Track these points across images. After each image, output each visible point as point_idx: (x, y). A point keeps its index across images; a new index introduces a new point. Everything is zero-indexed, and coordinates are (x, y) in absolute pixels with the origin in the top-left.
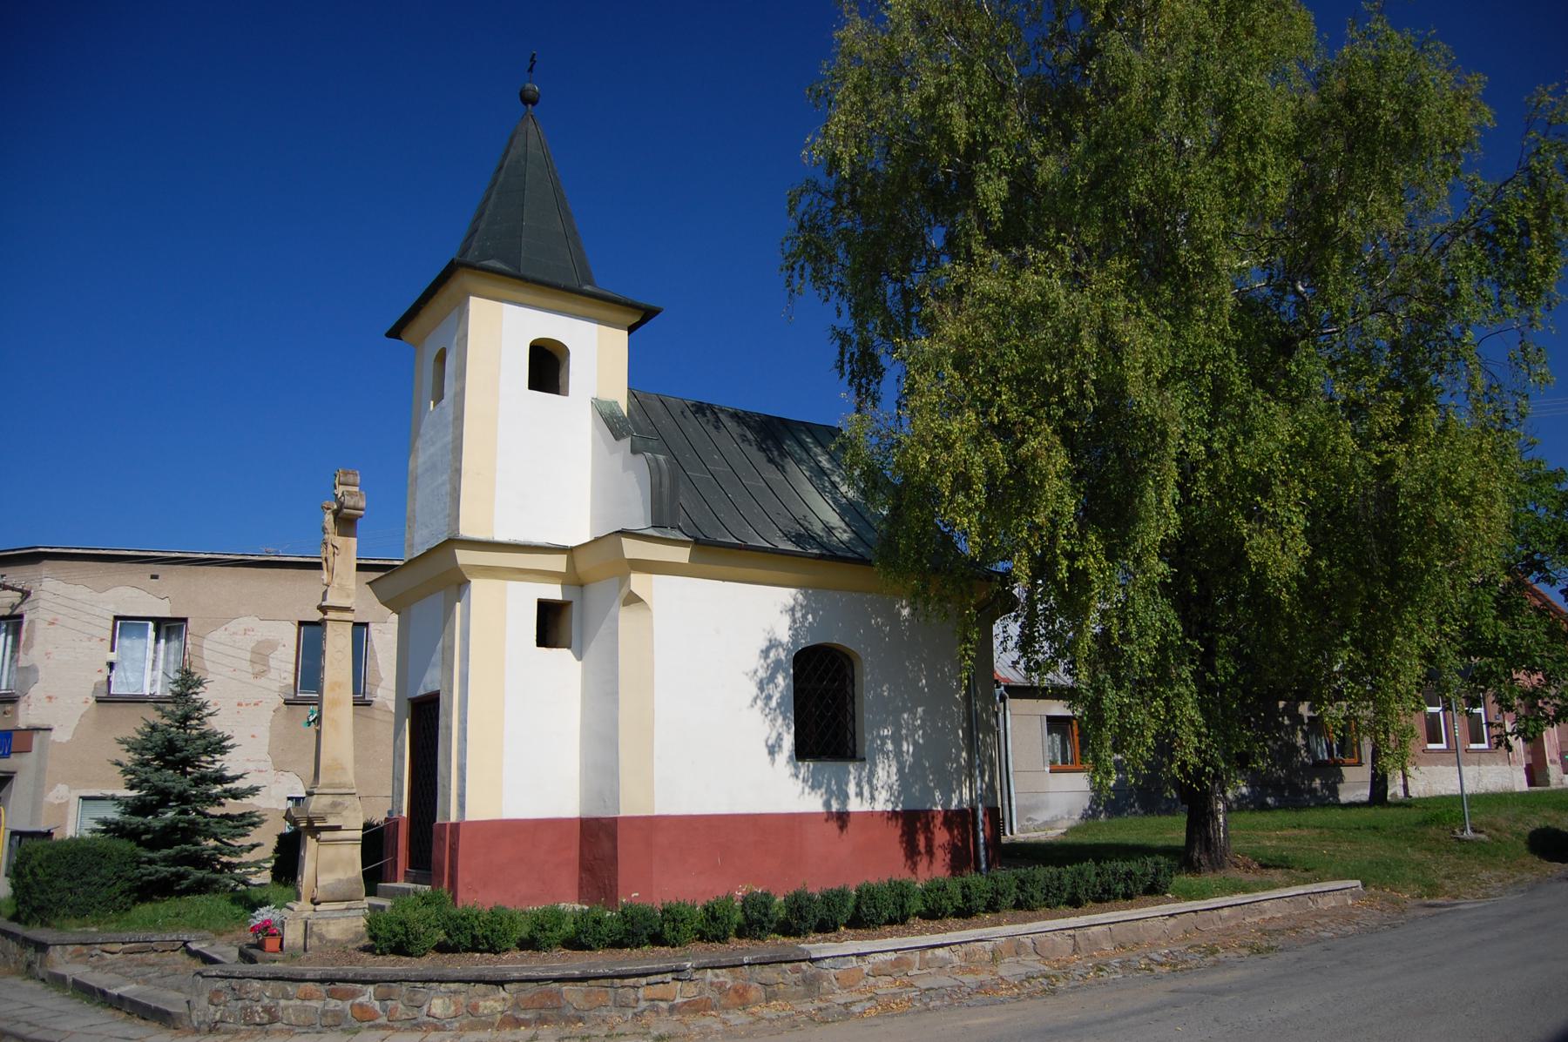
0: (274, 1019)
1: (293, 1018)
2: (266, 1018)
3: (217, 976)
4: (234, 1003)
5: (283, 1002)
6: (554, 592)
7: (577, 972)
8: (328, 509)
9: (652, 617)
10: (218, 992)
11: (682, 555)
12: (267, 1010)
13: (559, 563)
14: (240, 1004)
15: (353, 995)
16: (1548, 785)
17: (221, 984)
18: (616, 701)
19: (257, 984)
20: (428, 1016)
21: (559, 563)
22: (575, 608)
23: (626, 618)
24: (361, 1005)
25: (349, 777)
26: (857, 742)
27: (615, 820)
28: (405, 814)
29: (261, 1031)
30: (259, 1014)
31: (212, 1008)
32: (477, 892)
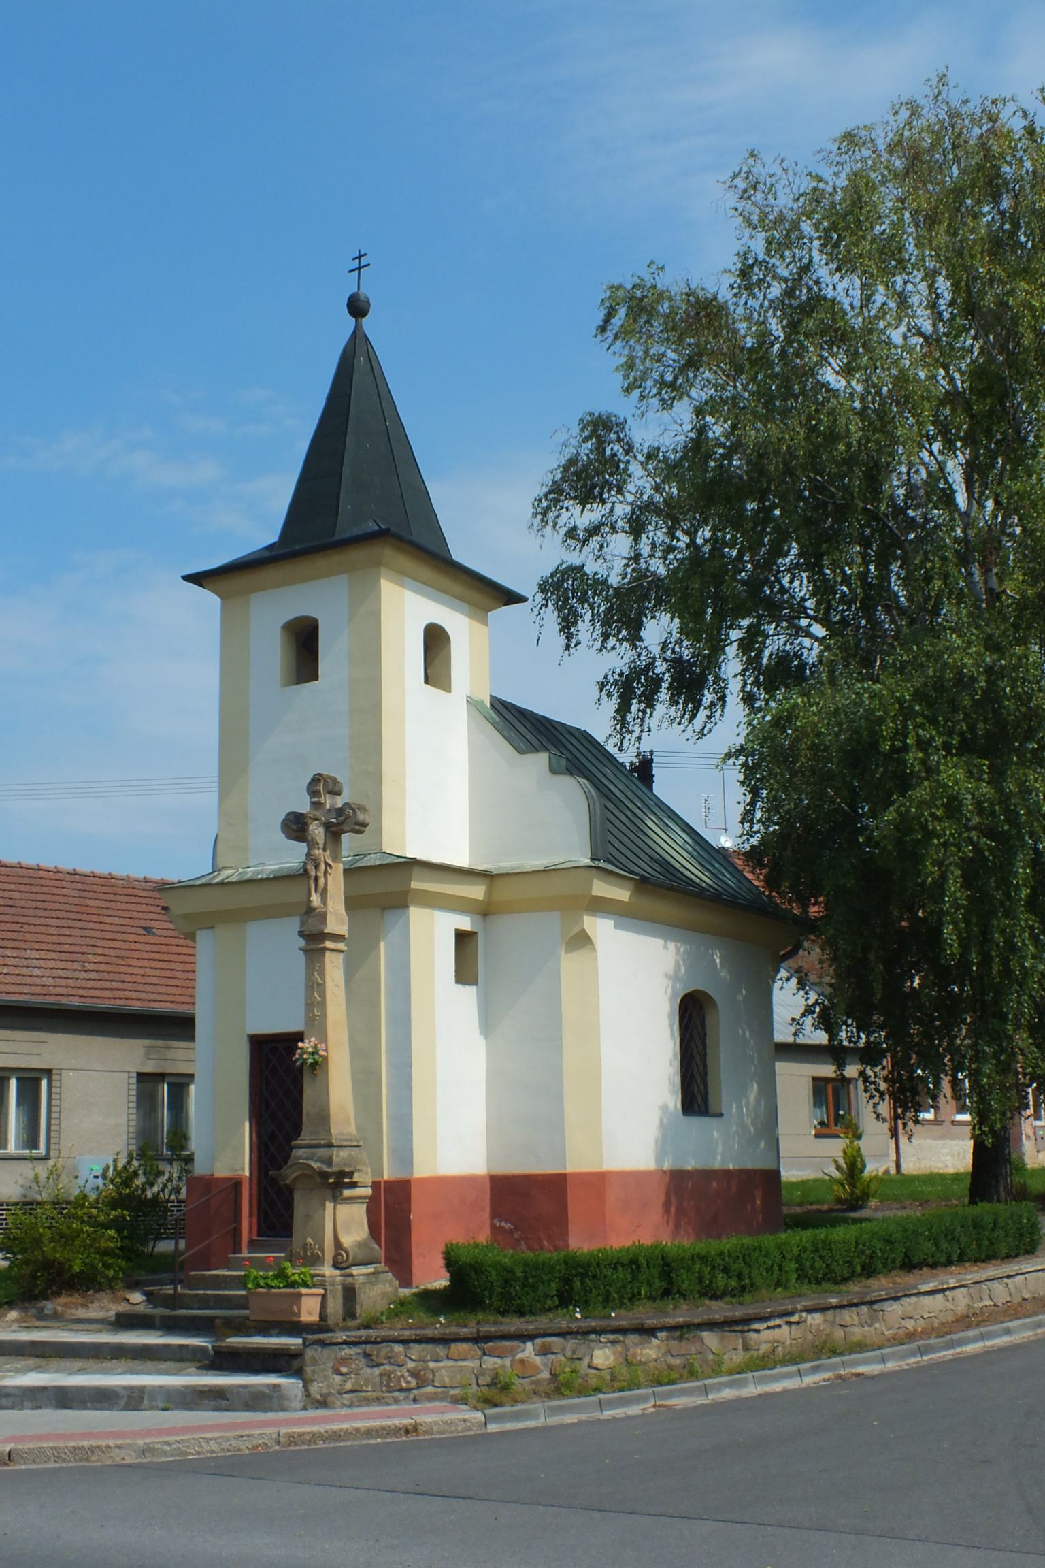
0: (422, 1382)
1: (447, 1380)
2: (414, 1383)
3: (345, 1343)
4: (369, 1370)
5: (432, 1365)
6: (465, 923)
7: (717, 1316)
8: (316, 819)
9: (596, 958)
10: (345, 1361)
11: (621, 894)
12: (414, 1374)
13: (476, 892)
14: (377, 1371)
15: (512, 1352)
16: (6, 1148)
17: (347, 1351)
18: (560, 1048)
19: (398, 1348)
20: (589, 1366)
21: (476, 892)
22: (480, 939)
23: (569, 963)
24: (522, 1361)
25: (352, 1129)
26: (709, 1090)
27: (563, 1177)
28: (247, 1173)
29: (407, 1398)
30: (405, 1379)
31: (338, 1378)
32: (424, 1257)
